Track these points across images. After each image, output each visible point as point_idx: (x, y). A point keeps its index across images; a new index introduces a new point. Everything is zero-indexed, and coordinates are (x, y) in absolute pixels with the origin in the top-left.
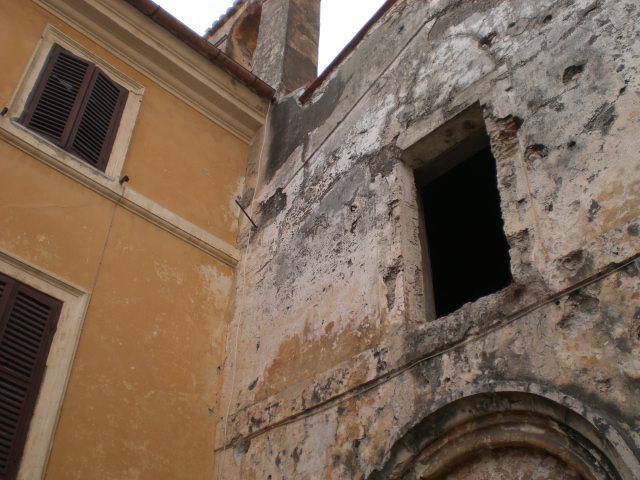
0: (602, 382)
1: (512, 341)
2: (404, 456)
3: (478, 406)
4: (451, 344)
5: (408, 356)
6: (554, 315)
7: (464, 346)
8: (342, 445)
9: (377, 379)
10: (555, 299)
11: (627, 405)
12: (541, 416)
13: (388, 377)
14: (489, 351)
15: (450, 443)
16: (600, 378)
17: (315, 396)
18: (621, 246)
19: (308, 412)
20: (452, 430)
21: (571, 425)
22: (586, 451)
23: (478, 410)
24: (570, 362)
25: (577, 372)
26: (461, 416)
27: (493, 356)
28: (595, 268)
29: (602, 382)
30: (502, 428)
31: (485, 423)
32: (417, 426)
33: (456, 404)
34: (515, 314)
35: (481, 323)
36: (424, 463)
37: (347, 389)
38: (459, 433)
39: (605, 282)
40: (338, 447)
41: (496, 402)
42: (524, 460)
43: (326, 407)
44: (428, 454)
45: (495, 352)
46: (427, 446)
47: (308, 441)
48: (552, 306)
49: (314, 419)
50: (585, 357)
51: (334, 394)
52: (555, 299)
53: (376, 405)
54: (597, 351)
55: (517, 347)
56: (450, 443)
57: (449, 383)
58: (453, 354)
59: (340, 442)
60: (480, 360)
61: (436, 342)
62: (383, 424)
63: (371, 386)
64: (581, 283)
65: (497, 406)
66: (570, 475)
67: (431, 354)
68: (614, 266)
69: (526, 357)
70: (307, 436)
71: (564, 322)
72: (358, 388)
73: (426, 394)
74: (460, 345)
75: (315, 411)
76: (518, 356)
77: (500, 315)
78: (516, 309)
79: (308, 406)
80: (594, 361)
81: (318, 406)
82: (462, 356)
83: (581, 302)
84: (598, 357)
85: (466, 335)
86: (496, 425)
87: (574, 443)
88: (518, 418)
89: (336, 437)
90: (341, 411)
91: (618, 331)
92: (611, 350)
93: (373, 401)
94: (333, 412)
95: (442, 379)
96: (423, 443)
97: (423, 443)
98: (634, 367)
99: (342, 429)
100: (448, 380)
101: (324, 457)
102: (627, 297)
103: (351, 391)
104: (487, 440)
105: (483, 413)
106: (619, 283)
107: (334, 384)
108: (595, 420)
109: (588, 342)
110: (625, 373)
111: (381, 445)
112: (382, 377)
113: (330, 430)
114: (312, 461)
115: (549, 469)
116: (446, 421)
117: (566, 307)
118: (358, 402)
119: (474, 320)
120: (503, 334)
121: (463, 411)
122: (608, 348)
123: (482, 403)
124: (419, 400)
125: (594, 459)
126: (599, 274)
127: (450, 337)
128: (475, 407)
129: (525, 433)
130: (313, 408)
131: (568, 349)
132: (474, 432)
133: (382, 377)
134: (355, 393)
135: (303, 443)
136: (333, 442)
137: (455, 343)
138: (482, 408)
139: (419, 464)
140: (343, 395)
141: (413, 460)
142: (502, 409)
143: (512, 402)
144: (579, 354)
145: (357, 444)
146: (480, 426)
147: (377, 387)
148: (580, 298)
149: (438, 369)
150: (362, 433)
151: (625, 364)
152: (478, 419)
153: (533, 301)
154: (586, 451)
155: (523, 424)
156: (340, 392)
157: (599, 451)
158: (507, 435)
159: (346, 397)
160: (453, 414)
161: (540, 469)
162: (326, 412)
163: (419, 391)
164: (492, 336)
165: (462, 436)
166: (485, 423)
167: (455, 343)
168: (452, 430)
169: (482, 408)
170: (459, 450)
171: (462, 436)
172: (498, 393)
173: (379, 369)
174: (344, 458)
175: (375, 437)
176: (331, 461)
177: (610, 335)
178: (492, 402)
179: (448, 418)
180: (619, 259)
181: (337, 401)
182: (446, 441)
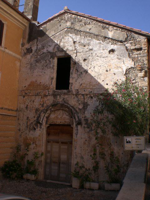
2: (51, 107)
4: (59, 95)
13: (49, 95)
46: (120, 45)
53: (47, 99)
63: (47, 96)
90: (41, 97)
91: (79, 102)
145: (44, 103)
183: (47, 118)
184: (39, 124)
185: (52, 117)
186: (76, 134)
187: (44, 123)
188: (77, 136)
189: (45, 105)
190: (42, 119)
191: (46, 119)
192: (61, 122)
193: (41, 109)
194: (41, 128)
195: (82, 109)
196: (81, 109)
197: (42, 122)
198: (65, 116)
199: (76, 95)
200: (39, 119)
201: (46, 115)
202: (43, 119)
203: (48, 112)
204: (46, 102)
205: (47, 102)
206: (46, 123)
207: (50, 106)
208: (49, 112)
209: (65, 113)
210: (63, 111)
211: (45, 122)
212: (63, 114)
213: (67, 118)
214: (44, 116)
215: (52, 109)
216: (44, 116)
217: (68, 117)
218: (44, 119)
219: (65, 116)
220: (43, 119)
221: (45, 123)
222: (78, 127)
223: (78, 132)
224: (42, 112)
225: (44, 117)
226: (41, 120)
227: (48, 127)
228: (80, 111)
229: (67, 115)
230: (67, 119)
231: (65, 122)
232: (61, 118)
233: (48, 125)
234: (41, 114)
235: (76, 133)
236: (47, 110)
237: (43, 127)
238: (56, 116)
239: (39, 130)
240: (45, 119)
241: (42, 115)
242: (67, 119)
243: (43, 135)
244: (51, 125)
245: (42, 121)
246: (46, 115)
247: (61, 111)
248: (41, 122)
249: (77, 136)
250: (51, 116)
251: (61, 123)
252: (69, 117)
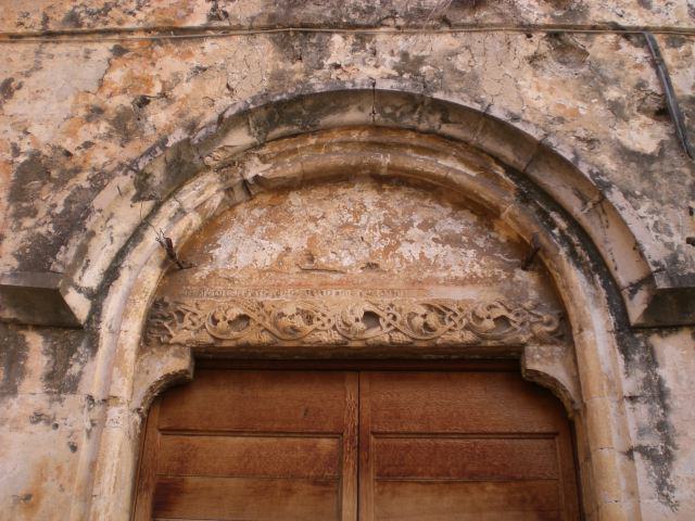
0: (583, 140)
1: (454, 54)
2: (240, 138)
3: (388, 110)
4: (352, 26)
5: (272, 17)
6: (524, 47)
7: (372, 35)
8: (110, 96)
9: (205, 29)
10: (528, 30)
11: (618, 175)
12: (479, 151)
13: (226, 32)
14: (414, 53)
15: (318, 146)
16: (582, 134)
17: (73, 18)
18: (628, 11)
19: (49, 36)
20: (328, 129)
21: (535, 174)
22: (545, 215)
23: (385, 115)
24: (540, 104)
25: (550, 118)
26: (353, 115)
27: (420, 61)
28: (591, 18)
29: (583, 140)
30: (409, 151)
31: (384, 138)
32: (279, 104)
33: (356, 94)
34: (464, 25)
35: (408, 17)
36: (264, 160)
37: (141, 25)
38: (337, 136)
39: (599, 39)
40: (102, 97)
41: (420, 113)
42: (426, 202)
43: (89, 38)
44: (276, 149)
45: (424, 57)
46: (282, 137)
47: (38, 76)
48: (521, 37)
49: (61, 49)
50: (564, 106)
51: (113, 25)
52: (528, 30)
53: (195, 62)
54: (580, 104)
55: (461, 62)
56: (318, 146)
57: (339, 71)
58: (351, 39)
59: (107, 91)
60: (397, 59)
61: (328, 14)
62: (203, 89)
63: (197, 34)
64: (569, 27)
65: (419, 121)
66: (497, 239)
67: (313, 26)
68: (616, 28)
69: (475, 77)
70: (38, 68)
71: (533, 60)
72: (166, 31)
73: (293, 72)
74: (369, 31)
75: (64, 38)
76: (462, 74)
77: (445, 21)
78: (469, 20)
79: (52, 27)
80: (575, 113)
81: (72, 34)
82: (368, 46)
83: (558, 48)
84: (582, 112)
85: (379, 24)
86: (403, 146)
87: (524, 199)
88: (440, 145)
89: (101, 84)
90: (119, 51)
91: (612, 94)
92: (600, 110)
93: (190, 54)
94: (103, 49)
95: (328, 62)
96: (278, 132)
97: (278, 132)
98: (631, 139)
99: (117, 76)
100: (337, 66)
101: (68, 104)
102: (628, 65)
103: (147, 31)
104: (385, 160)
105: (391, 122)
106: (618, 47)
107: (115, 12)
108: (590, 172)
109: (569, 91)
110: (618, 142)
111: (194, 114)
112: (213, 29)
113: (90, 73)
114: (39, 105)
115: (466, 224)
116: (327, 113)
117: (539, 43)
118: (158, 48)
119: (399, 10)
120: (443, 42)
121: (361, 109)
122: (597, 106)
123: (397, 109)
124: (278, 76)
125: (553, 225)
126: (594, 27)
127: (352, 16)
128: (381, 110)
129: (124, 314)
130: (63, 33)
131: (539, 89)
132: (360, 143)
133: (213, 29)
134: (155, 34)
135: (27, 75)
136: (94, 87)
137: (358, 27)
138: (391, 115)
139: (256, 160)
140: (130, 31)
141: (248, 151)
142: (424, 126)
143: (445, 120)
144: (554, 99)
145: (144, 102)
146: (375, 139)
147: (201, 39)
148: (559, 43)
149: (323, 50)
150: (158, 88)
151: (619, 131)
152: (375, 128)
153: (496, 20)
154: (545, 215)
155: (446, 155)
156: (127, 26)
157: (566, 214)
158: (417, 162)
159: (136, 36)
160: (344, 109)
161: (450, 220)
162: (89, 46)
163: (281, 66)
164: (422, 38)
165: (341, 143)
166: (384, 138)
167: (358, 27)
168: (328, 129)
169: (391, 115)
170: (336, 159)
171: (341, 143)
172: (437, 100)
173: (211, 18)
174: (112, 115)
175: (183, 100)
176: (82, 112)
177: (601, 95)
178: (413, 112)
179: (333, 110)
180: (623, 22)
181: (116, 37)
182: (312, 141)
183: (176, 262)
184: (35, 341)
185: (242, 259)
186: (646, 452)
187: (122, 321)
188: (662, 485)
189: (159, 117)
190: (100, 259)
191: (152, 277)
192: (370, 316)
193: (99, 158)
194: (60, 382)
195: (661, 154)
196: (650, 158)
197: (96, 311)
198: (433, 251)
199: (554, 35)
200: (68, 254)
201: (171, 226)
202: (112, 274)
203: (189, 196)
204: (177, 92)
205: (184, 90)
206: (154, 333)
207: (243, 116)
208: (204, 192)
209: (417, 218)
210: (397, 200)
211: (141, 306)
212: (395, 231)
213: (458, 272)
214: (136, 236)
215: (255, 169)
216: (136, 236)
217: (466, 262)
218: (125, 277)
219: (418, 246)
220: (112, 274)
221: (133, 329)
222: (651, 361)
223: (673, 419)
224: (125, 181)
225: (121, 254)
226: (91, 278)
227: (170, 392)
228: (646, 175)
229: (450, 240)
230: (457, 282)
231: (441, 310)
232: (371, 266)
233: (173, 363)
234: (99, 201)
235: (653, 441)
236: (182, 169)
237: (94, 373)
238: (297, 243)
239: (38, 417)
240: (143, 272)
241: (117, 214)
242: (457, 282)
243: (88, 497)
244: (211, 363)
245: (97, 296)
246: (161, 227)
247: (369, 197)
248: (78, 304)
249: (662, 485)
250: (220, 253)
251: (379, 335)
252: (481, 253)
